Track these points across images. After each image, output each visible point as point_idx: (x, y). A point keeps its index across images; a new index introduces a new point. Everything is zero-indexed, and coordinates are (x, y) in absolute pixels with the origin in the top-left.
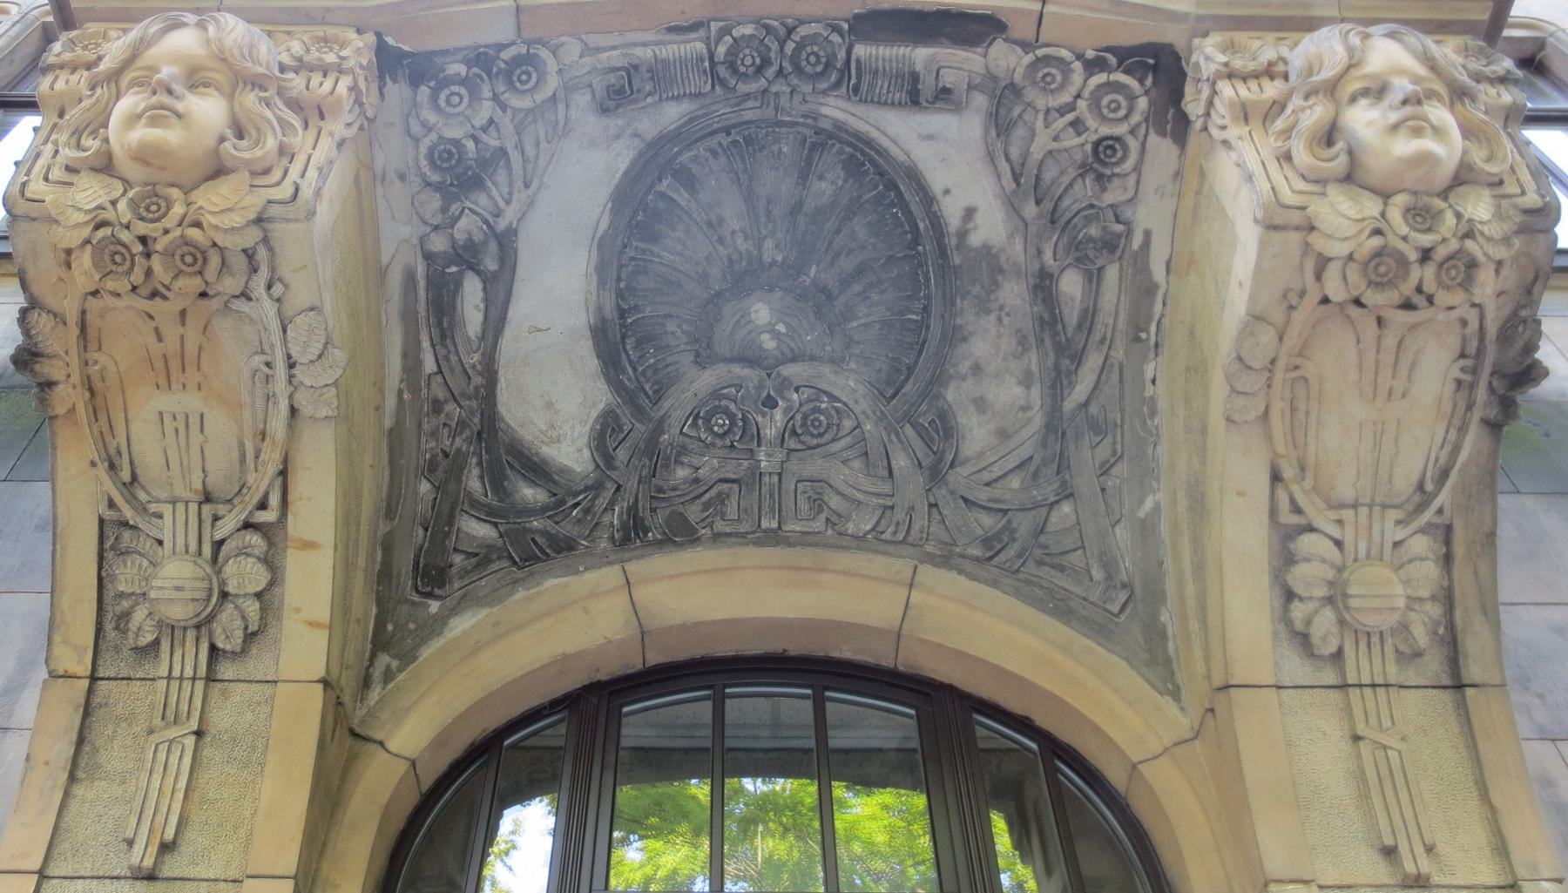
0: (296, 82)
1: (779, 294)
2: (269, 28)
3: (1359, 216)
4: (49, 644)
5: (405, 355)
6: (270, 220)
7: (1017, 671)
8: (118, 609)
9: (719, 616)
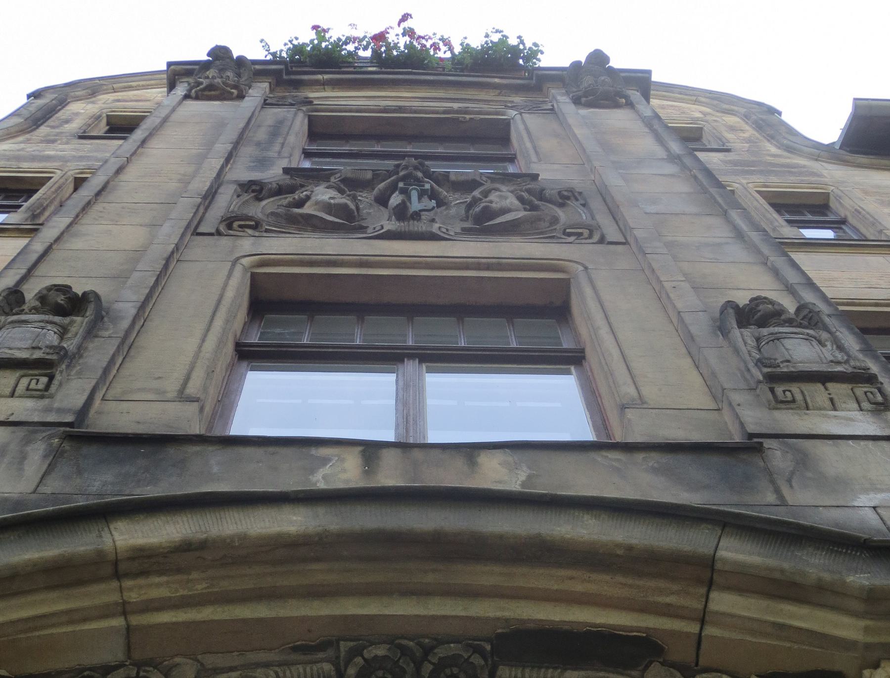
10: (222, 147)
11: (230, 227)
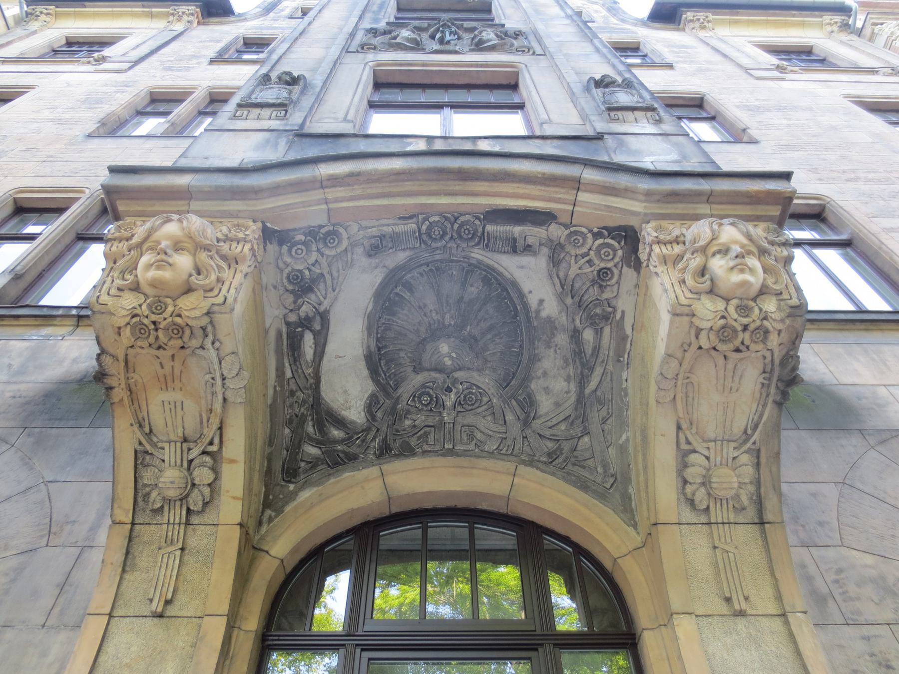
0: (225, 247)
1: (452, 339)
2: (212, 220)
3: (715, 310)
4: (112, 508)
5: (277, 370)
6: (213, 313)
7: (562, 515)
8: (144, 492)
9: (425, 490)
10: (357, 13)
11: (363, 48)
